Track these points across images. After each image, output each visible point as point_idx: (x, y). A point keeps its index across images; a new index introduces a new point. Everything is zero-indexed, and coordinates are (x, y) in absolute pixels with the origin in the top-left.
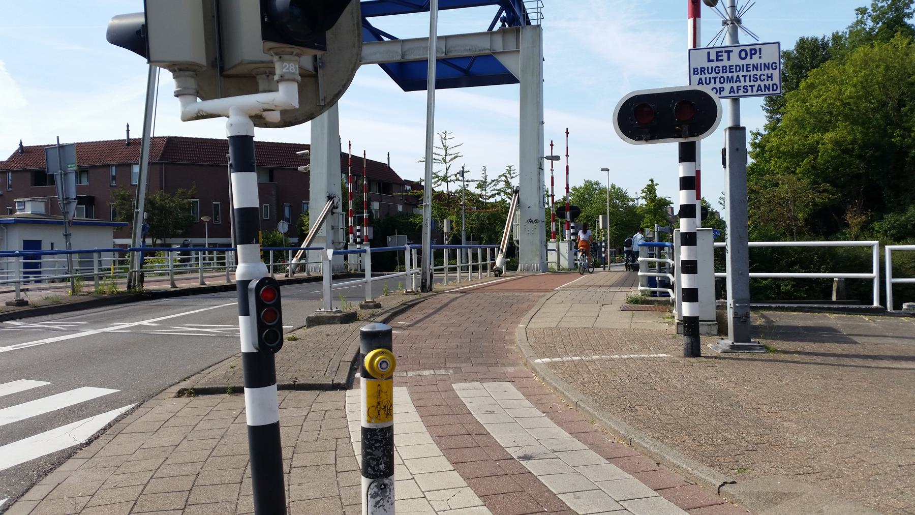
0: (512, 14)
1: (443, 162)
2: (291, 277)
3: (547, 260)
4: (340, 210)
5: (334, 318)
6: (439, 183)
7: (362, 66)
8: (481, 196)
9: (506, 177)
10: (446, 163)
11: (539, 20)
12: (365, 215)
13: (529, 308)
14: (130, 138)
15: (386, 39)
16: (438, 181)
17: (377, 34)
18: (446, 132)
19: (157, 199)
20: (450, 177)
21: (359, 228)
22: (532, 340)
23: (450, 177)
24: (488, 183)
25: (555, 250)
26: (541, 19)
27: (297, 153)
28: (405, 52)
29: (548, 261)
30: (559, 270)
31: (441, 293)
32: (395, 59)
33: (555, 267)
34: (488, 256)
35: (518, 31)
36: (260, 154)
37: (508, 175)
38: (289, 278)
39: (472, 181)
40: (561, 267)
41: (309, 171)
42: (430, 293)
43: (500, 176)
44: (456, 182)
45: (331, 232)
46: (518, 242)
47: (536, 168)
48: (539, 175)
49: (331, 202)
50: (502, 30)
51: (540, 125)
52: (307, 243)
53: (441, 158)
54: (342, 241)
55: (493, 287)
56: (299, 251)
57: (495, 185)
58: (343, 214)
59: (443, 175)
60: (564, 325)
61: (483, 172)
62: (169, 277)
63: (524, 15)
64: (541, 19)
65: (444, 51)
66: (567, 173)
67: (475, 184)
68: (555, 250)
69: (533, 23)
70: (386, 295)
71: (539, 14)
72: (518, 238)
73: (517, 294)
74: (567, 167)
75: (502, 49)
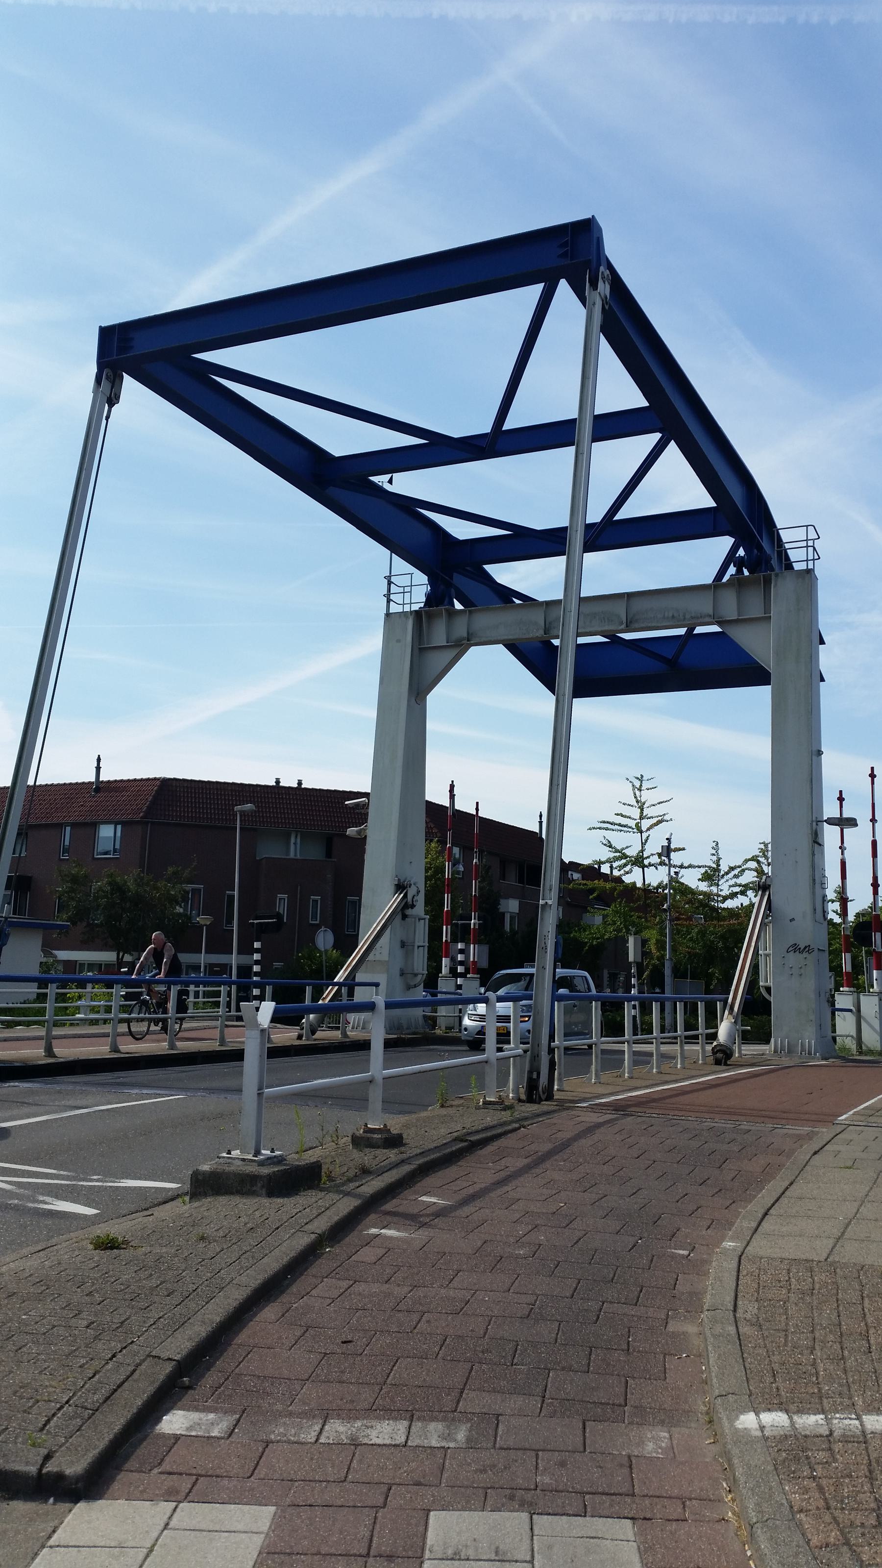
0: (756, 551)
1: (635, 830)
2: (307, 1040)
3: (834, 1031)
4: (420, 909)
5: (253, 1179)
6: (627, 868)
7: (473, 649)
8: (708, 895)
9: (758, 862)
10: (641, 832)
11: (811, 557)
12: (473, 921)
13: (768, 1173)
14: (101, 780)
15: (517, 601)
16: (625, 865)
17: (506, 595)
18: (642, 776)
19: (131, 885)
20: (648, 857)
21: (463, 947)
22: (748, 1308)
23: (648, 857)
24: (722, 873)
25: (850, 1010)
26: (814, 560)
27: (346, 803)
28: (550, 623)
29: (838, 1033)
30: (861, 1053)
31: (568, 1108)
32: (531, 635)
33: (851, 1044)
34: (701, 1020)
35: (767, 582)
36: (305, 805)
37: (762, 860)
38: (303, 1042)
39: (690, 866)
40: (864, 1048)
41: (366, 836)
42: (545, 1106)
43: (746, 861)
44: (659, 867)
45: (399, 952)
46: (768, 990)
47: (805, 842)
48: (813, 854)
49: (402, 895)
50: (738, 582)
51: (814, 758)
52: (347, 973)
53: (632, 823)
54: (421, 971)
55: (703, 1098)
56: (330, 987)
57: (736, 876)
58: (424, 919)
59: (635, 854)
60: (849, 1253)
61: (714, 852)
62: (42, 1032)
63: (780, 554)
64: (814, 560)
65: (625, 621)
66: (875, 854)
67: (698, 873)
68: (850, 1010)
69: (797, 567)
70: (442, 1106)
71: (811, 549)
72: (770, 983)
73: (745, 1126)
74: (874, 844)
75: (736, 613)
